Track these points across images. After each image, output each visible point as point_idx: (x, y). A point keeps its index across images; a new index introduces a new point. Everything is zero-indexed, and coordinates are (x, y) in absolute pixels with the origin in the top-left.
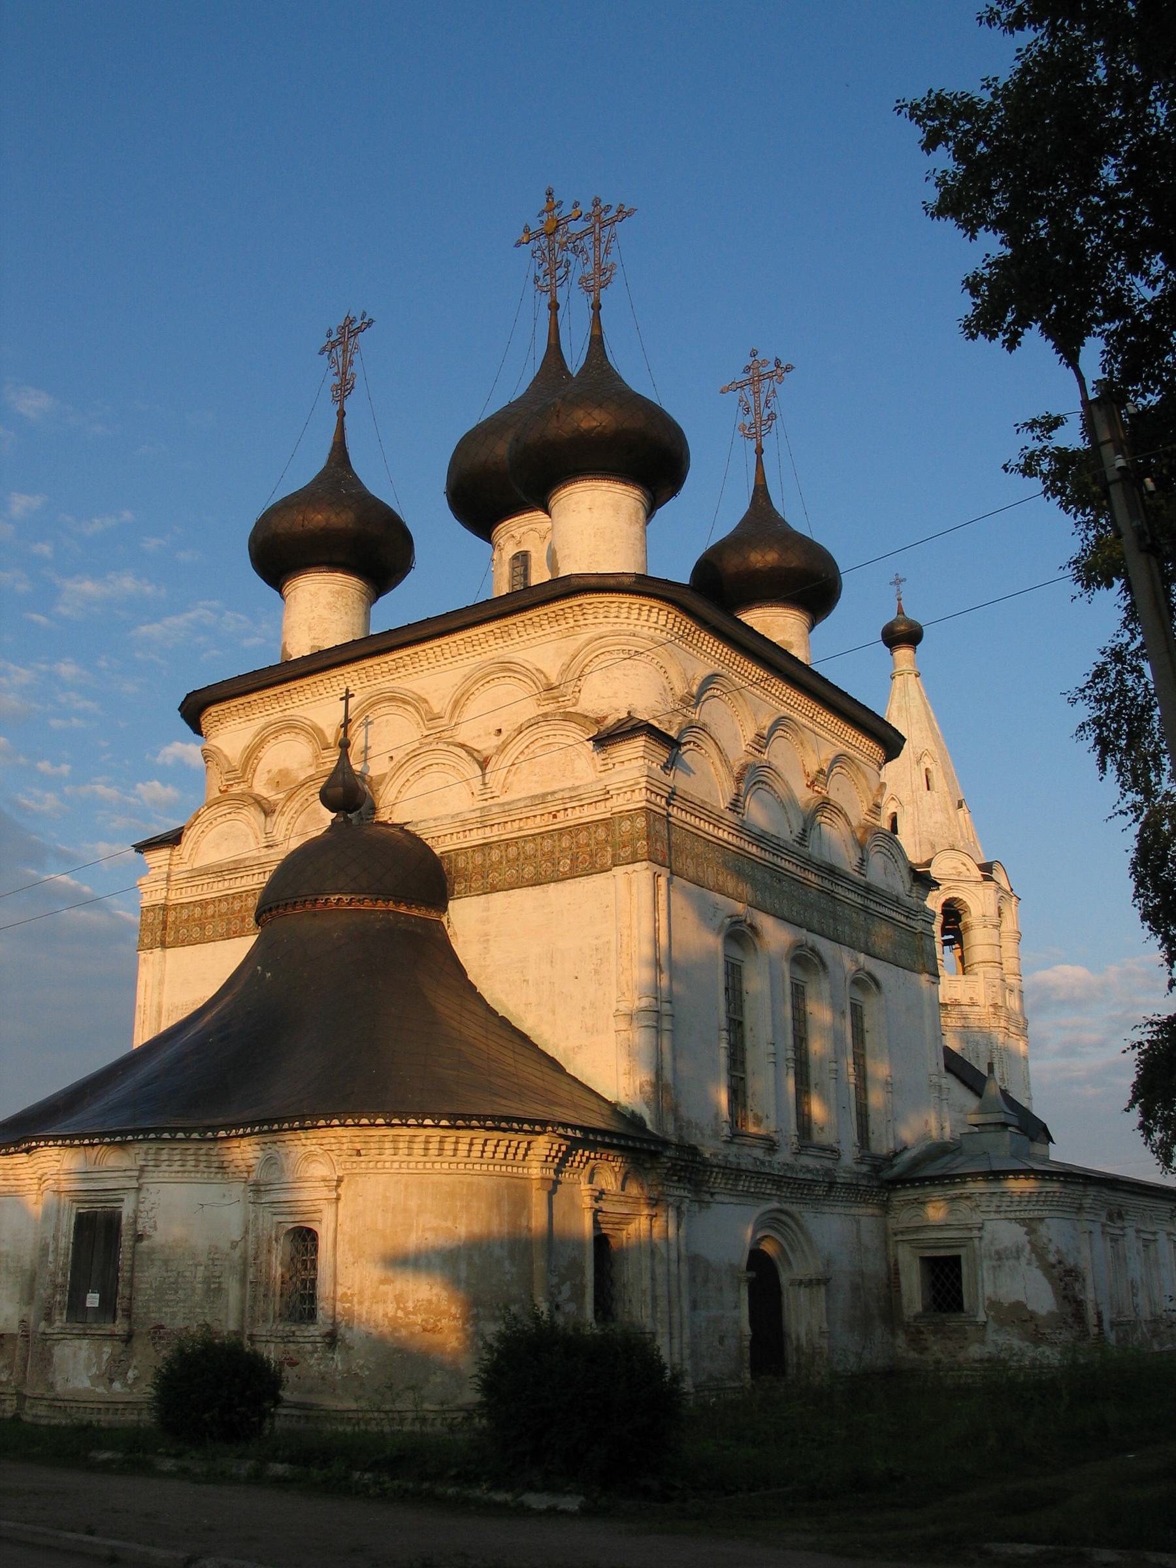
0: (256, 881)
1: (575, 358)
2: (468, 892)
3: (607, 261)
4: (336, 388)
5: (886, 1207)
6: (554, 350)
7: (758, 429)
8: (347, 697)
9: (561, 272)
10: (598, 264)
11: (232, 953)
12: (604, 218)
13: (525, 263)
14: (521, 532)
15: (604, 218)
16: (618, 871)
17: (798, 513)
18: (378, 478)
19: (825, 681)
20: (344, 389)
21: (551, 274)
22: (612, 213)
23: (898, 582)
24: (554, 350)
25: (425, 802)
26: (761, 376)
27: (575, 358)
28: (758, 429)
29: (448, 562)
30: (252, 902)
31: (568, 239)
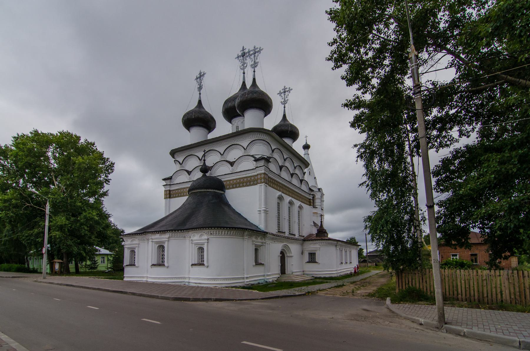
0: (189, 185)
1: (249, 85)
2: (229, 188)
3: (257, 61)
4: (199, 88)
5: (302, 245)
6: (244, 84)
7: (284, 103)
8: (204, 151)
9: (245, 65)
10: (255, 62)
11: (183, 200)
12: (256, 51)
13: (238, 63)
14: (237, 121)
15: (256, 51)
16: (259, 185)
17: (291, 120)
18: (208, 107)
19: (175, 211)
20: (200, 88)
21: (243, 67)
22: (258, 50)
23: (306, 137)
24: (244, 84)
25: (221, 171)
26: (285, 91)
27: (249, 85)
28: (284, 103)
29: (223, 127)
30: (188, 189)
31: (248, 56)
